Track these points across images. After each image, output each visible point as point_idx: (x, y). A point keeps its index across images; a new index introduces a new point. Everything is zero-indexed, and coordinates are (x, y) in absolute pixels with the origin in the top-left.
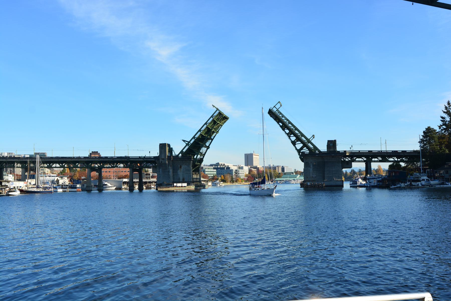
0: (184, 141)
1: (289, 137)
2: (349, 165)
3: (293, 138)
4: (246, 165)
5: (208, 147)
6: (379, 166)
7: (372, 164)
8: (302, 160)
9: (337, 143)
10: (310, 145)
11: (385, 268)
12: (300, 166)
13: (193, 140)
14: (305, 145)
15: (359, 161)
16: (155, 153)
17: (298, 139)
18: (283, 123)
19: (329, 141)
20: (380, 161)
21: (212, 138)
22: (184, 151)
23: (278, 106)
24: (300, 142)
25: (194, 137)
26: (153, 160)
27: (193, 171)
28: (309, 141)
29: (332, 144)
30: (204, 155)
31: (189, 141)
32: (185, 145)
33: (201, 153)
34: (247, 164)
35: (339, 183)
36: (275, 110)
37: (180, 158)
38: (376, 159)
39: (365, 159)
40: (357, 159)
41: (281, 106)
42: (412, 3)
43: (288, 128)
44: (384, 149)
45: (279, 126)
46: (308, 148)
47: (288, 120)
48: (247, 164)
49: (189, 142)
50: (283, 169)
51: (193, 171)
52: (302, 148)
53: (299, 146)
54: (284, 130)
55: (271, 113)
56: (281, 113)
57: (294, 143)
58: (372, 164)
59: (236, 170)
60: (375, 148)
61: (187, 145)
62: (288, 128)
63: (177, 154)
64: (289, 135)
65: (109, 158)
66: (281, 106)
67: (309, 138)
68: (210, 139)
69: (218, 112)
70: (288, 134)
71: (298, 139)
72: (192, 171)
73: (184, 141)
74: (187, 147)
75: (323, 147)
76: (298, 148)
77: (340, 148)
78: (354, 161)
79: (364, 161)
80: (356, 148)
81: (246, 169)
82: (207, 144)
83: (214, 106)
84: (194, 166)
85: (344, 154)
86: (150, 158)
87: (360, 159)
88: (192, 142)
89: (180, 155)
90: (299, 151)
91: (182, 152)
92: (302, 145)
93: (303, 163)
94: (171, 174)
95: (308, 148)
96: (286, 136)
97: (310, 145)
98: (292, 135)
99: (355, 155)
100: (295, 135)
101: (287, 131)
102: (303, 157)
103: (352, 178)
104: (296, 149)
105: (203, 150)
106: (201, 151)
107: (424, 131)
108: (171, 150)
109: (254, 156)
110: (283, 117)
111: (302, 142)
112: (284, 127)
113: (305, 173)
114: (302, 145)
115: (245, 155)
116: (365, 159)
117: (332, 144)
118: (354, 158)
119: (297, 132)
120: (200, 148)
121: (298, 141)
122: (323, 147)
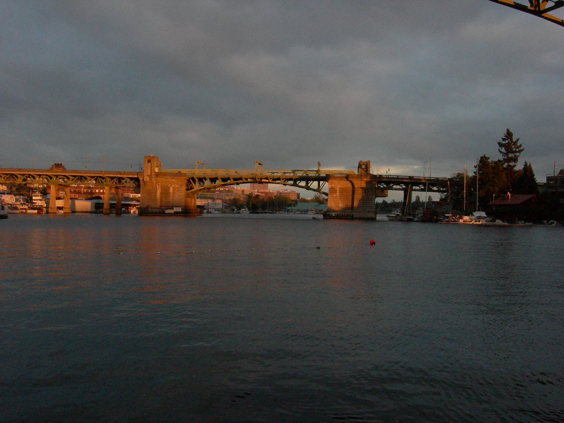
2: (383, 193)
7: (310, 187)
11: (506, 224)
22: (425, 178)
38: (417, 188)
39: (404, 187)
40: (395, 187)
73: (465, 170)
78: (391, 188)
79: (403, 189)
87: (398, 187)
116: (404, 187)
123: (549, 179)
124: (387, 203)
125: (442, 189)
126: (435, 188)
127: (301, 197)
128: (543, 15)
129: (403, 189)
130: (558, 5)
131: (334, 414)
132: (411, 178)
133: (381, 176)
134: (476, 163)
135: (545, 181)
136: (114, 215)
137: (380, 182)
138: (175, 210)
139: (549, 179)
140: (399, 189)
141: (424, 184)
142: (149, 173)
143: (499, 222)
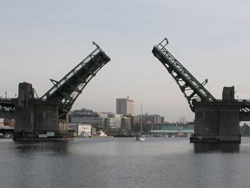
0: (52, 80)
1: (177, 81)
3: (182, 83)
4: (117, 113)
5: (80, 92)
6: (245, 124)
8: (193, 109)
9: (235, 90)
10: (201, 90)
12: (191, 116)
13: (63, 82)
14: (196, 91)
16: (13, 93)
17: (188, 84)
18: (171, 65)
19: (225, 88)
22: (51, 93)
23: (164, 44)
24: (189, 88)
25: (65, 78)
26: (11, 103)
27: (60, 118)
28: (201, 86)
29: (229, 92)
30: (75, 100)
31: (58, 81)
34: (119, 112)
36: (160, 47)
37: (44, 102)
43: (176, 71)
45: (165, 68)
46: (200, 95)
47: (184, 69)
48: (119, 112)
49: (58, 83)
50: (163, 118)
51: (60, 118)
53: (189, 92)
54: (170, 72)
55: (156, 52)
56: (167, 52)
57: (183, 89)
59: (106, 119)
61: (55, 86)
62: (176, 71)
63: (40, 96)
64: (177, 79)
68: (84, 82)
69: (98, 51)
70: (175, 78)
71: (188, 84)
72: (58, 117)
73: (52, 80)
74: (55, 90)
75: (218, 96)
76: (188, 95)
77: (238, 96)
81: (118, 117)
82: (80, 88)
83: (94, 43)
84: (60, 112)
86: (7, 100)
88: (62, 83)
89: (45, 97)
90: (189, 98)
91: (47, 94)
92: (192, 91)
93: (194, 114)
95: (200, 95)
96: (173, 79)
97: (201, 90)
100: (184, 79)
101: (175, 74)
102: (195, 106)
104: (186, 96)
105: (75, 94)
108: (32, 91)
109: (128, 102)
110: (177, 64)
111: (193, 87)
112: (171, 68)
113: (195, 124)
114: (192, 91)
117: (229, 92)
119: (186, 75)
120: (70, 92)
121: (187, 87)
122: (218, 96)
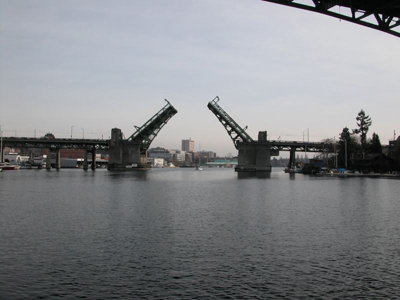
0: (135, 127)
1: (226, 127)
2: (276, 153)
3: (229, 129)
5: (156, 135)
6: (274, 158)
7: (296, 152)
8: (237, 148)
11: (362, 174)
12: (235, 153)
13: (144, 128)
14: (239, 135)
15: (285, 150)
16: (107, 136)
17: (233, 129)
18: (221, 116)
19: (260, 132)
20: (302, 151)
21: (160, 127)
22: (135, 136)
24: (234, 132)
25: (145, 125)
28: (243, 131)
29: (263, 135)
31: (140, 127)
32: (136, 130)
33: (149, 140)
34: (183, 150)
35: (268, 168)
36: (213, 103)
38: (299, 149)
39: (290, 148)
40: (284, 149)
41: (219, 99)
42: (339, 19)
43: (225, 120)
44: (306, 141)
46: (242, 137)
48: (183, 150)
49: (140, 128)
50: (215, 154)
52: (236, 138)
53: (234, 135)
54: (221, 121)
55: (210, 106)
56: (218, 107)
57: (230, 133)
58: (296, 153)
59: (174, 155)
60: (300, 139)
61: (138, 131)
62: (225, 120)
63: (127, 138)
64: (225, 126)
65: (92, 141)
66: (219, 99)
67: (243, 128)
68: (159, 128)
69: (169, 106)
70: (224, 125)
71: (233, 129)
73: (135, 127)
74: (137, 133)
75: (255, 138)
76: (234, 137)
77: (270, 138)
78: (281, 150)
79: (289, 150)
80: (284, 139)
81: (183, 153)
82: (155, 132)
83: (166, 100)
84: (141, 149)
85: (274, 143)
86: (103, 141)
87: (286, 149)
88: (142, 129)
89: (131, 139)
90: (234, 140)
91: (132, 136)
93: (238, 151)
94: (325, 156)
95: (242, 137)
96: (223, 127)
98: (228, 126)
99: (281, 145)
100: (231, 126)
101: (224, 122)
102: (238, 145)
103: (277, 164)
104: (232, 138)
105: (152, 136)
106: (149, 138)
107: (348, 129)
108: (121, 135)
109: (190, 142)
111: (237, 132)
112: (221, 118)
113: (238, 158)
115: (183, 141)
116: (290, 148)
117: (263, 135)
118: (281, 147)
119: (232, 123)
120: (148, 135)
122: (255, 138)
123: (390, 142)
124: (276, 159)
125: (316, 150)
126: (312, 150)
127: (217, 155)
128: (331, 10)
129: (289, 150)
130: (398, 23)
131: (294, 294)
132: (295, 142)
133: (274, 141)
134: (341, 132)
135: (388, 144)
136: (45, 169)
137: (274, 146)
138: (133, 165)
139: (390, 142)
140: (287, 150)
141: (304, 147)
142: (115, 141)
143: (357, 173)
